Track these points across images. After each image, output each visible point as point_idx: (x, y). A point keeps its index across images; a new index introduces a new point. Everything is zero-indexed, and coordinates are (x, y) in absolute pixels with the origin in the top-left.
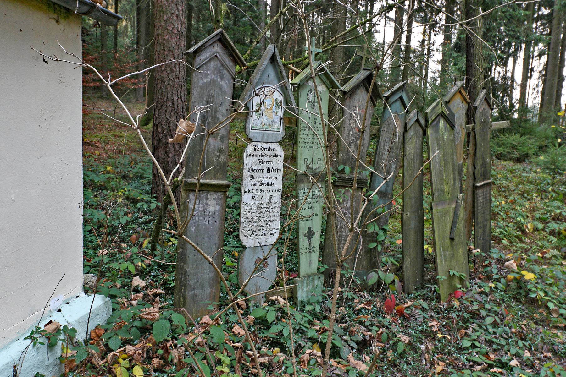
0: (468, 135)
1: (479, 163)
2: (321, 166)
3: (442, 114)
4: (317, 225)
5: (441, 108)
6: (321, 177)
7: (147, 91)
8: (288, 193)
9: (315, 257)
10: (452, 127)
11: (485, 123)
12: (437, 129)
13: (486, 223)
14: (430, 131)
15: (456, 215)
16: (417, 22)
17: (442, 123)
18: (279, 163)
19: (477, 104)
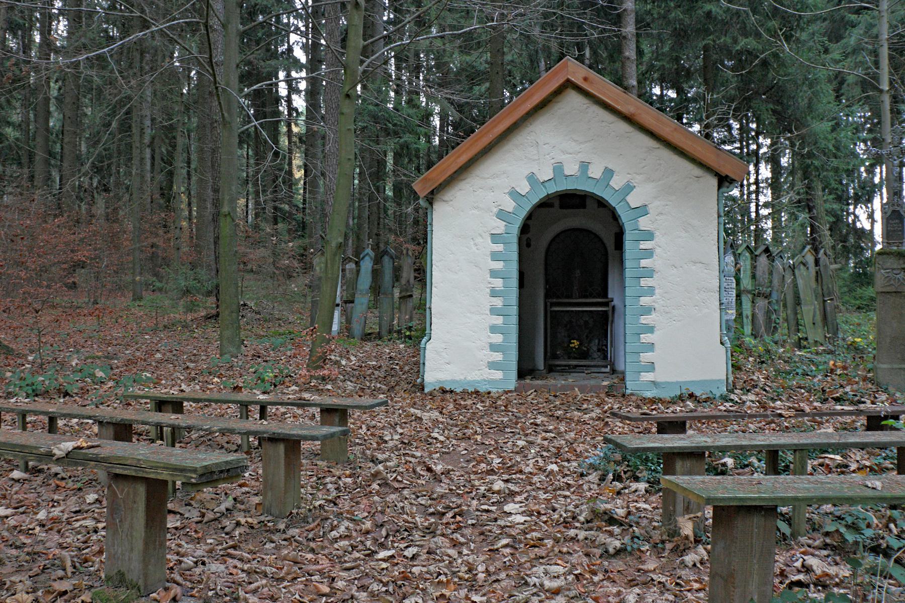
0: (817, 273)
1: (825, 288)
2: (750, 287)
3: (802, 263)
4: (749, 313)
5: (801, 259)
6: (749, 292)
7: (560, 300)
8: (738, 296)
9: (750, 327)
10: (808, 268)
11: (826, 266)
12: (799, 270)
13: (716, 122)
14: (796, 271)
15: (815, 312)
16: (680, 515)
17: (802, 267)
18: (734, 285)
19: (820, 256)
